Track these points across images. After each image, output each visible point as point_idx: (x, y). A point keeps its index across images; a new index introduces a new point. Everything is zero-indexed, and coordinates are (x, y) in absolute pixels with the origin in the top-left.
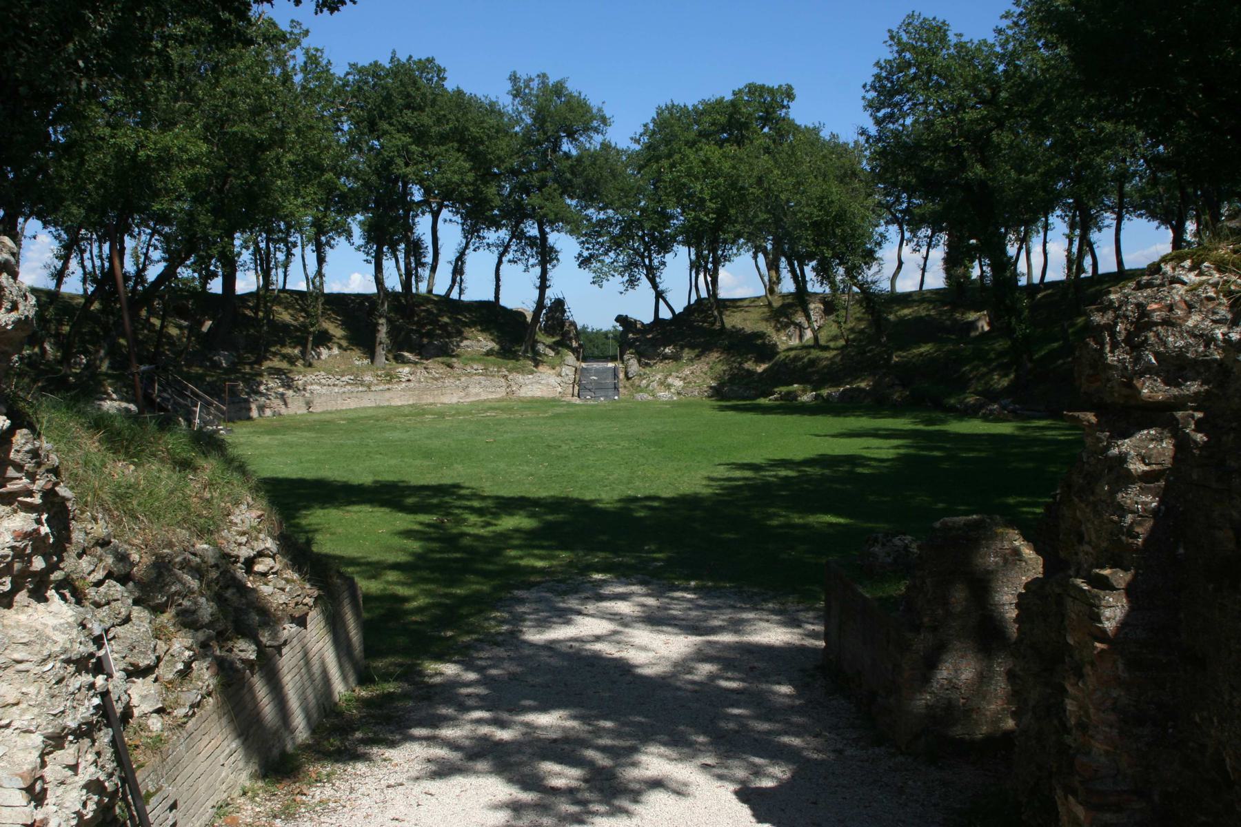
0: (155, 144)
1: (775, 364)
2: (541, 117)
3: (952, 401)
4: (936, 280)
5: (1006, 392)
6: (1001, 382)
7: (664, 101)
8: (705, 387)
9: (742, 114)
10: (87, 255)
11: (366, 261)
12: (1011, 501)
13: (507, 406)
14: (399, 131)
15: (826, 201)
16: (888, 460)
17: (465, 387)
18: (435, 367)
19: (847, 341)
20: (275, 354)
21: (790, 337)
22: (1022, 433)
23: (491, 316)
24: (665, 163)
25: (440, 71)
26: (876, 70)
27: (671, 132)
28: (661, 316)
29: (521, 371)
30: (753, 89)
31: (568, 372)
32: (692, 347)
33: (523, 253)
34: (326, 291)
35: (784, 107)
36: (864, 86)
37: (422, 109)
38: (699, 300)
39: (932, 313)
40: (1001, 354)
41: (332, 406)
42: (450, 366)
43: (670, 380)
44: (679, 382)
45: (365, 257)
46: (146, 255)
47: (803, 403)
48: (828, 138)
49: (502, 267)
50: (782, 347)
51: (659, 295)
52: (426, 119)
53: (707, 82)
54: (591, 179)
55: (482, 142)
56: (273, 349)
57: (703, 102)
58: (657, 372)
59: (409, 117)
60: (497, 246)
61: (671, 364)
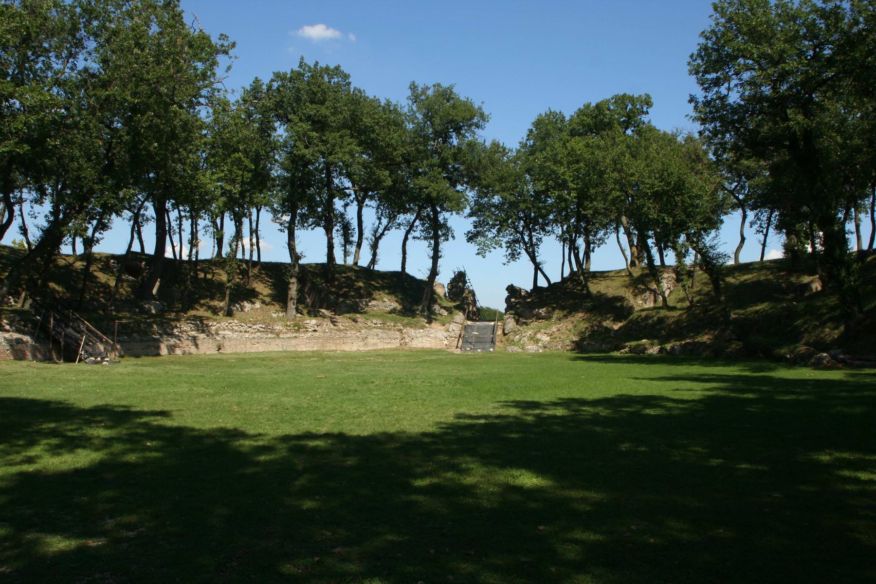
1: (629, 323)
3: (783, 351)
4: (775, 253)
5: (836, 343)
6: (831, 333)
8: (568, 342)
9: (604, 115)
11: (281, 230)
12: (825, 458)
15: (666, 174)
16: (687, 401)
17: (370, 337)
18: (343, 321)
19: (691, 302)
20: (202, 305)
21: (645, 301)
22: (851, 379)
25: (346, 77)
26: (703, 41)
28: (539, 284)
29: (414, 326)
32: (562, 308)
35: (643, 113)
36: (691, 56)
38: (572, 273)
39: (771, 277)
40: (833, 309)
41: (241, 349)
42: (355, 321)
43: (539, 336)
45: (280, 227)
47: (651, 355)
49: (408, 243)
50: (637, 308)
51: (538, 267)
54: (477, 168)
55: (373, 131)
56: (202, 302)
61: (543, 323)
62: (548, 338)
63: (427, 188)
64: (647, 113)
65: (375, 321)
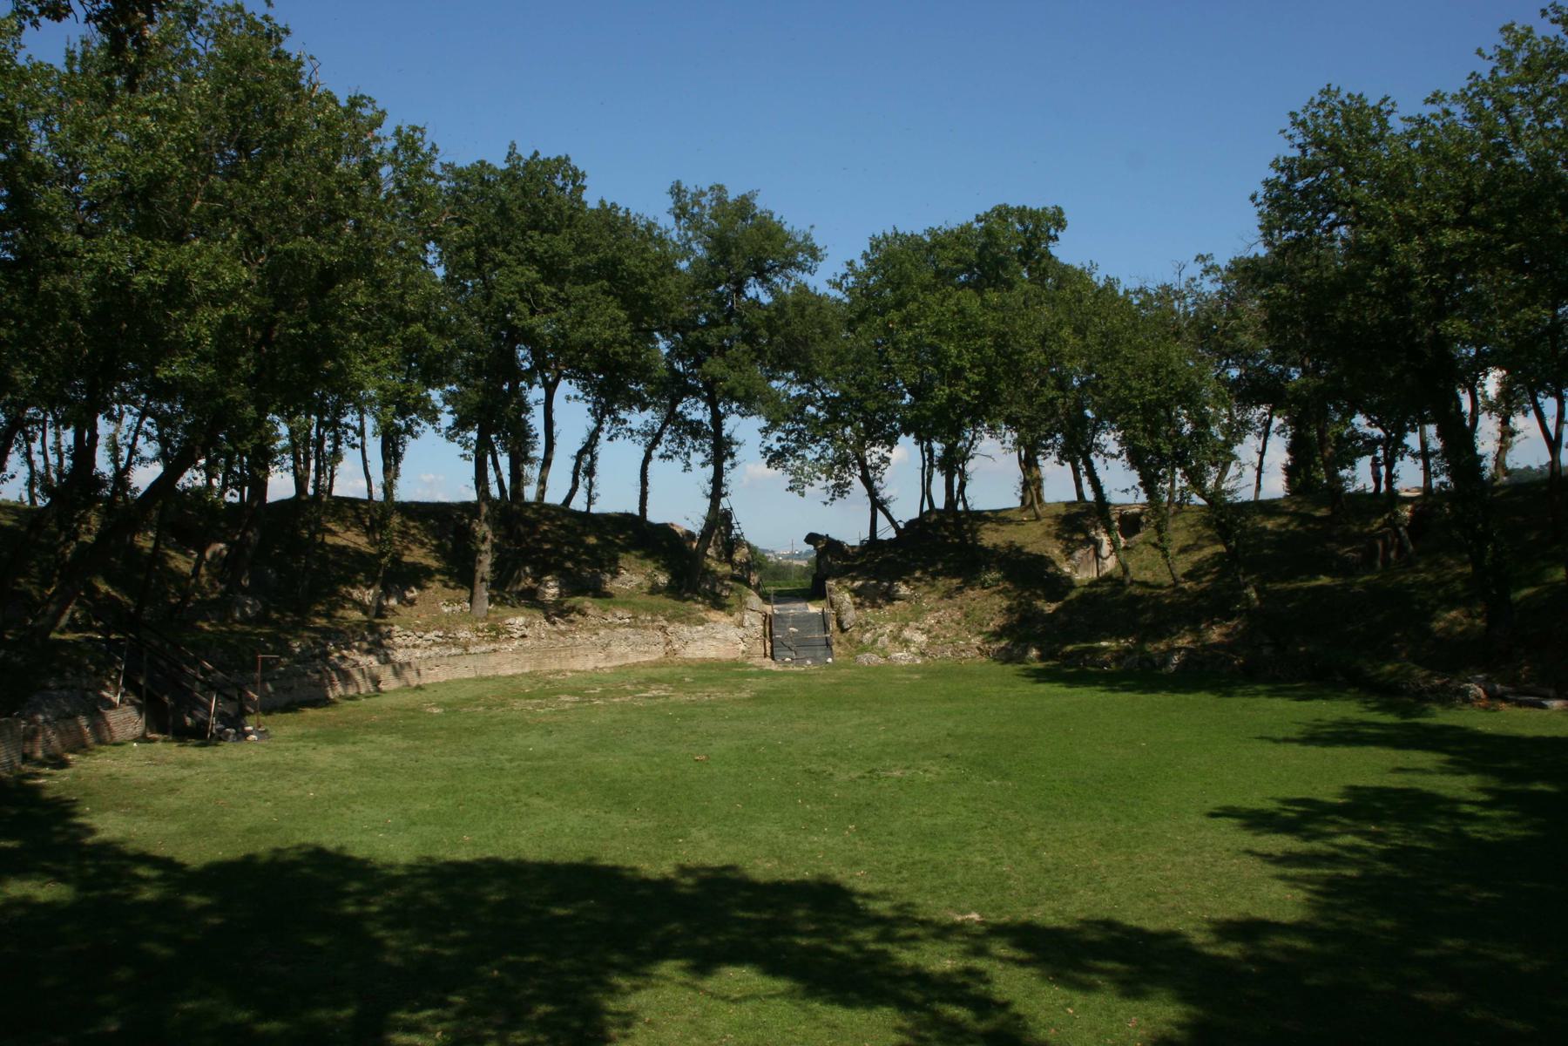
0: (163, 264)
2: (721, 246)
7: (882, 227)
10: (36, 446)
13: (673, 673)
14: (520, 263)
15: (1163, 372)
17: (613, 647)
23: (637, 534)
24: (894, 315)
25: (577, 176)
27: (898, 268)
30: (1002, 213)
31: (753, 620)
33: (682, 443)
34: (336, 492)
35: (1050, 238)
37: (556, 232)
43: (907, 633)
44: (919, 634)
45: (461, 450)
46: (133, 450)
48: (1101, 284)
49: (650, 465)
51: (878, 504)
52: (562, 244)
53: (943, 203)
54: (789, 339)
57: (932, 232)
58: (883, 623)
59: (538, 243)
60: (645, 434)
62: (924, 637)
63: (725, 380)
64: (1056, 238)
65: (619, 614)
